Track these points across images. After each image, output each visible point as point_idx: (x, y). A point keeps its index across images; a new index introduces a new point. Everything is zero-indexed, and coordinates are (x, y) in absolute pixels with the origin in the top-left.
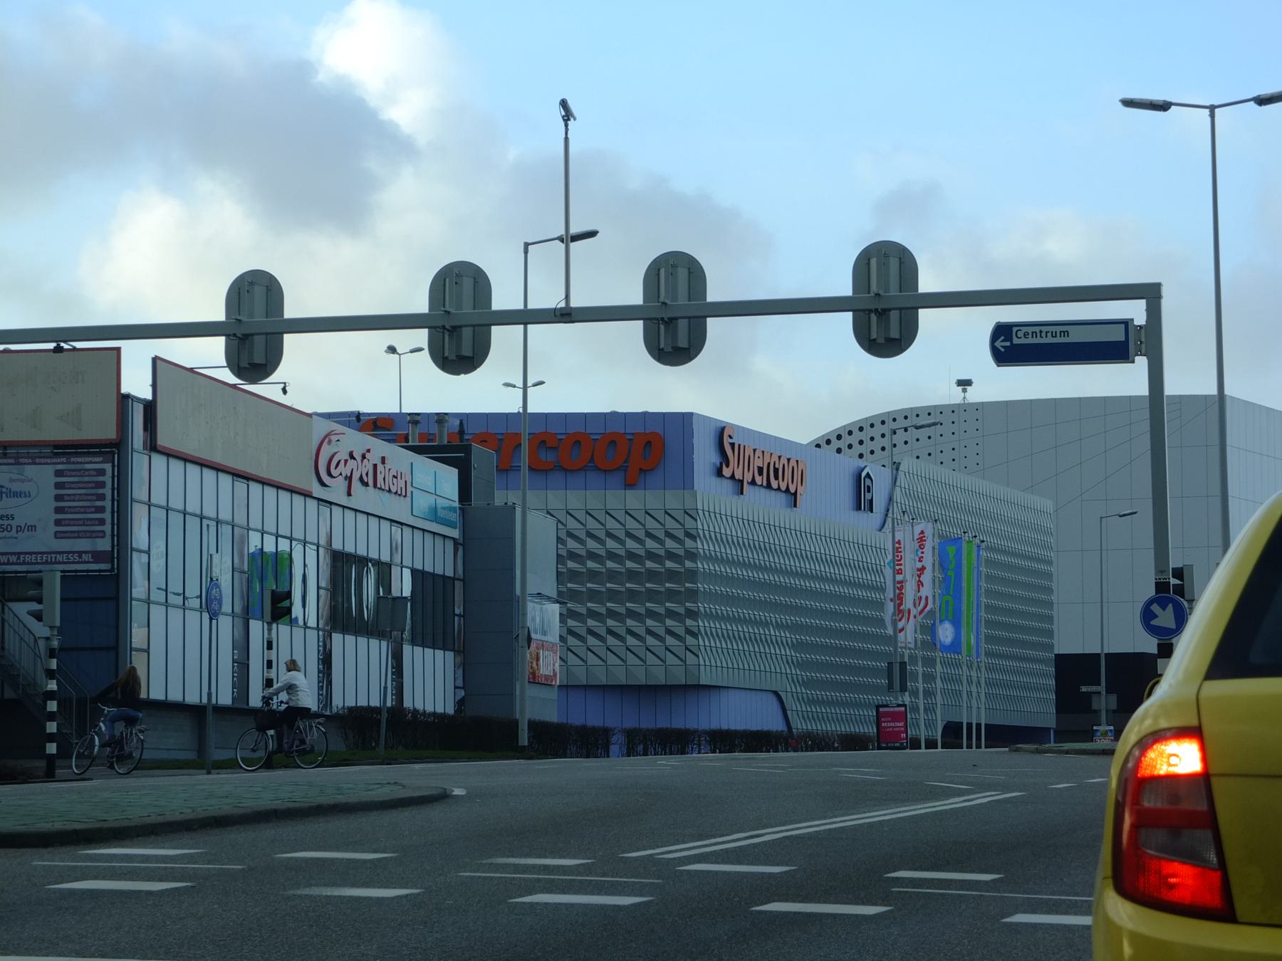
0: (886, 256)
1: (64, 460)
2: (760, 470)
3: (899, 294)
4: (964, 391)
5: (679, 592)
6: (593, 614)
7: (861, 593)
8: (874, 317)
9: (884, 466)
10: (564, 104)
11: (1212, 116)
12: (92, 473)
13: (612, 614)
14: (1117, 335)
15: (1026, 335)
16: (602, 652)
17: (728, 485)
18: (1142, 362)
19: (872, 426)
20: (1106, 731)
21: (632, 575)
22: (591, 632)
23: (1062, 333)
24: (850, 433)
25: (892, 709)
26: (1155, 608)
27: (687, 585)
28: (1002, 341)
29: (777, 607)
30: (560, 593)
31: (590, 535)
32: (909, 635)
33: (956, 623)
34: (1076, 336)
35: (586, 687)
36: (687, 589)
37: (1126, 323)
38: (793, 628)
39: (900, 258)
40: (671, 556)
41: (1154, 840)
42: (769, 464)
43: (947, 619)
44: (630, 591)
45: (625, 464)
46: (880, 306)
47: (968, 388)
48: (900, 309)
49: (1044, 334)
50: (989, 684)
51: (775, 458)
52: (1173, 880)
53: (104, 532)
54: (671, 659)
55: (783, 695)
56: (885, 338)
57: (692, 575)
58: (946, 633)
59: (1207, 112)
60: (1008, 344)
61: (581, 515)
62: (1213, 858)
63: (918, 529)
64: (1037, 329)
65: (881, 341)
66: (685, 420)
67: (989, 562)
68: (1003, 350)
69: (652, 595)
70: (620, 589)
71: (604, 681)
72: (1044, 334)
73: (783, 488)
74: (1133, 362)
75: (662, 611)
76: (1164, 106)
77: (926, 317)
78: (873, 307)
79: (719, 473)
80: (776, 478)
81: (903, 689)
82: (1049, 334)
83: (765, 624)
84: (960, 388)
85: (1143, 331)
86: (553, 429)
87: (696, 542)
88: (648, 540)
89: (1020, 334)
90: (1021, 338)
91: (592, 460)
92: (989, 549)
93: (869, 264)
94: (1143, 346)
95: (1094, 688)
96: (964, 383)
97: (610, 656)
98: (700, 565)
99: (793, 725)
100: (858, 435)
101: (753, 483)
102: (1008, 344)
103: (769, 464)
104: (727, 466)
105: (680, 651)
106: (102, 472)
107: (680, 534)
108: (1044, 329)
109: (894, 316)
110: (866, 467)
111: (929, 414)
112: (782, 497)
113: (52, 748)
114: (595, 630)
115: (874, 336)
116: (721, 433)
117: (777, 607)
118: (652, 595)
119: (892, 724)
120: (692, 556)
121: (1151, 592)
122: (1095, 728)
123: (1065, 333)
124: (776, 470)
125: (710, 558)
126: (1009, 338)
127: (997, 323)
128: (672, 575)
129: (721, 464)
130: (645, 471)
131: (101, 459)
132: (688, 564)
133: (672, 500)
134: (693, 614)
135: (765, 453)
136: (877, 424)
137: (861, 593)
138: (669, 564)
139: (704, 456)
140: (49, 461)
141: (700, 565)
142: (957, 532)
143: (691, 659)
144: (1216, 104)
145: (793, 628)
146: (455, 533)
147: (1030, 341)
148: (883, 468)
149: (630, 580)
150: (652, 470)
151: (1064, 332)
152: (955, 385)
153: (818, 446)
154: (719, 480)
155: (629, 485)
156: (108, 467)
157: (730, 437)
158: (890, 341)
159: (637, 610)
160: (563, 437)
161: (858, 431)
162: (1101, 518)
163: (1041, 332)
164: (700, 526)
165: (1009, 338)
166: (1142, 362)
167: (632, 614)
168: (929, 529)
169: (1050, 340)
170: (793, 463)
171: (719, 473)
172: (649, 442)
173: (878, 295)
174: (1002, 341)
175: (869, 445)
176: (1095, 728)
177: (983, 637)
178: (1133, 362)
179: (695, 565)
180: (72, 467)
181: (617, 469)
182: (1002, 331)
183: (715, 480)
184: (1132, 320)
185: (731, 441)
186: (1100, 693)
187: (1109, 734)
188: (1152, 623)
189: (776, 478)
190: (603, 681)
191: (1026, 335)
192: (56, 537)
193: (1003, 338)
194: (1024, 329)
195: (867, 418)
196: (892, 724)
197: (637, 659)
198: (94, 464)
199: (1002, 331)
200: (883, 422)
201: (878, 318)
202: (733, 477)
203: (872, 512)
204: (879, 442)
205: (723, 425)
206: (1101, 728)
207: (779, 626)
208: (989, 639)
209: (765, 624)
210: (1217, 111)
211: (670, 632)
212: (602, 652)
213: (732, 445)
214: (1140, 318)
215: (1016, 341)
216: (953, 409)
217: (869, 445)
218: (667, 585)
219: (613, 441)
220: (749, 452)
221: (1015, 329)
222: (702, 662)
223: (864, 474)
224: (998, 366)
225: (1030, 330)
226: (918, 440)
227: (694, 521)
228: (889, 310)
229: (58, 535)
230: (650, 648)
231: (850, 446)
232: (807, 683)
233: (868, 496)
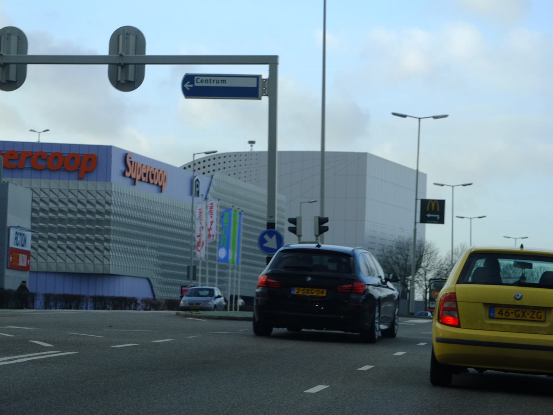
0: (128, 34)
2: (145, 174)
3: (134, 55)
4: (252, 146)
5: (102, 230)
6: (60, 238)
13: (69, 239)
14: (252, 84)
15: (202, 81)
16: (64, 256)
17: (128, 181)
18: (265, 100)
21: (80, 221)
22: (59, 247)
23: (222, 81)
26: (266, 237)
28: (189, 84)
29: (150, 239)
30: (33, 227)
31: (60, 201)
32: (202, 253)
33: (227, 249)
34: (229, 83)
35: (47, 273)
36: (106, 229)
37: (258, 77)
38: (159, 249)
39: (136, 36)
40: (98, 212)
41: (445, 313)
42: (149, 172)
43: (223, 246)
44: (60, 227)
45: (78, 169)
46: (122, 62)
48: (135, 64)
49: (212, 81)
50: (243, 277)
51: (152, 169)
52: (449, 320)
54: (96, 261)
55: (151, 280)
56: (125, 81)
57: (108, 222)
58: (222, 253)
60: (191, 86)
61: (57, 192)
62: (456, 316)
63: (209, 203)
64: (208, 78)
65: (123, 82)
66: (108, 149)
67: (246, 221)
68: (188, 89)
69: (89, 231)
70: (46, 226)
71: (55, 270)
72: (212, 81)
73: (156, 183)
74: (260, 99)
75: (84, 238)
77: (149, 69)
78: (118, 62)
79: (124, 175)
80: (153, 178)
82: (215, 81)
83: (144, 246)
85: (267, 82)
86: (45, 150)
89: (199, 81)
90: (199, 83)
91: (63, 165)
92: (245, 214)
93: (118, 39)
94: (267, 90)
96: (252, 143)
97: (77, 259)
99: (156, 294)
100: (202, 164)
101: (141, 180)
102: (191, 86)
103: (149, 172)
104: (128, 171)
105: (101, 258)
107: (103, 202)
108: (213, 78)
109: (131, 67)
112: (155, 188)
114: (61, 246)
115: (119, 79)
116: (126, 156)
118: (89, 231)
120: (109, 213)
121: (265, 229)
123: (224, 81)
124: (153, 175)
126: (192, 82)
127: (186, 74)
128: (98, 222)
129: (125, 170)
130: (88, 172)
132: (107, 217)
133: (100, 186)
134: (108, 240)
135: (148, 167)
139: (117, 166)
142: (229, 205)
143: (106, 261)
145: (159, 249)
147: (204, 84)
149: (79, 223)
150: (91, 172)
151: (224, 80)
153: (185, 168)
154: (124, 178)
155: (80, 178)
157: (130, 158)
159: (100, 238)
163: (210, 80)
164: (113, 199)
166: (265, 100)
167: (88, 240)
168: (215, 203)
170: (161, 172)
171: (124, 175)
173: (121, 55)
174: (189, 84)
177: (240, 256)
178: (260, 99)
181: (75, 171)
182: (188, 79)
183: (121, 178)
184: (261, 76)
185: (131, 160)
188: (265, 245)
189: (153, 178)
190: (64, 270)
191: (202, 81)
193: (188, 82)
194: (201, 78)
199: (188, 79)
201: (122, 69)
202: (130, 177)
204: (212, 168)
205: (127, 152)
207: (151, 248)
208: (244, 256)
209: (144, 246)
211: (97, 248)
212: (64, 256)
213: (131, 162)
214: (265, 75)
215: (196, 84)
216: (246, 154)
219: (73, 157)
220: (139, 166)
221: (196, 78)
222: (111, 263)
223: (195, 179)
224: (186, 98)
225: (205, 78)
228: (128, 64)
231: (199, 169)
232: (164, 275)
233: (197, 189)
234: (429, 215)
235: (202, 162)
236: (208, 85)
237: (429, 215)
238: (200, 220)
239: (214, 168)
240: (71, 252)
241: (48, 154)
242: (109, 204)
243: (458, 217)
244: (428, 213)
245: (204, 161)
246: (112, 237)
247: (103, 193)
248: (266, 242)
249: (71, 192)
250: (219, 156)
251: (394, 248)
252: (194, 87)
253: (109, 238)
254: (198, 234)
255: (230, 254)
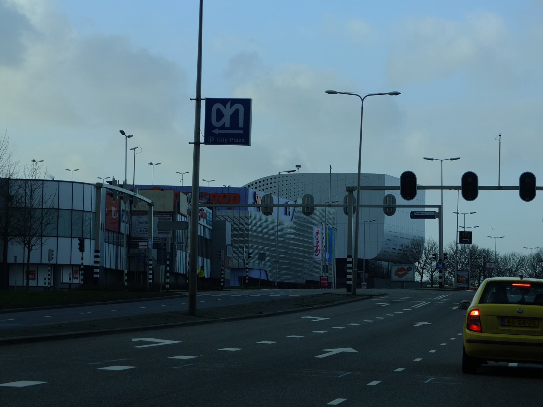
1: (160, 215)
4: (298, 169)
7: (271, 237)
8: (388, 209)
9: (252, 188)
10: (330, 166)
11: (442, 162)
12: (168, 219)
18: (437, 219)
19: (271, 179)
20: (364, 284)
24: (260, 182)
25: (324, 278)
26: (439, 264)
27: (246, 239)
29: (266, 245)
34: (426, 214)
37: (435, 212)
40: (241, 230)
47: (300, 168)
53: (170, 233)
57: (247, 236)
59: (441, 161)
65: (389, 213)
74: (436, 219)
76: (432, 159)
81: (327, 272)
84: (297, 168)
87: (248, 226)
88: (240, 225)
95: (361, 272)
96: (298, 166)
98: (249, 233)
100: (262, 183)
106: (170, 219)
107: (244, 223)
108: (420, 212)
109: (391, 208)
110: (288, 202)
111: (287, 177)
113: (222, 284)
117: (266, 245)
119: (324, 282)
120: (247, 230)
122: (361, 283)
123: (424, 213)
125: (252, 231)
128: (241, 236)
131: (170, 216)
132: (246, 232)
133: (242, 213)
136: (269, 179)
137: (271, 237)
138: (240, 232)
140: (157, 216)
141: (249, 233)
144: (443, 160)
146: (211, 228)
148: (259, 191)
152: (295, 167)
156: (171, 218)
158: (391, 213)
160: (210, 194)
161: (262, 181)
162: (365, 222)
165: (414, 214)
166: (437, 219)
169: (421, 214)
172: (235, 196)
175: (266, 186)
176: (361, 283)
178: (436, 219)
179: (248, 233)
180: (162, 217)
182: (412, 213)
186: (363, 273)
187: (365, 285)
191: (417, 213)
192: (158, 234)
195: (266, 177)
196: (324, 282)
197: (236, 260)
198: (168, 217)
200: (271, 179)
203: (289, 215)
204: (270, 185)
206: (363, 283)
210: (443, 161)
214: (437, 211)
215: (415, 214)
217: (266, 186)
218: (240, 238)
226: (283, 185)
227: (248, 220)
229: (159, 233)
230: (234, 257)
234: (464, 240)
235: (262, 181)
236: (419, 215)
237: (464, 240)
238: (317, 237)
239: (271, 185)
240: (236, 255)
241: (209, 194)
242: (248, 224)
243: (460, 227)
244: (463, 238)
245: (264, 181)
246: (250, 245)
247: (244, 218)
248: (439, 265)
249: (229, 217)
250: (275, 177)
251: (410, 245)
252: (414, 215)
253: (248, 246)
254: (316, 246)
255: (326, 255)
